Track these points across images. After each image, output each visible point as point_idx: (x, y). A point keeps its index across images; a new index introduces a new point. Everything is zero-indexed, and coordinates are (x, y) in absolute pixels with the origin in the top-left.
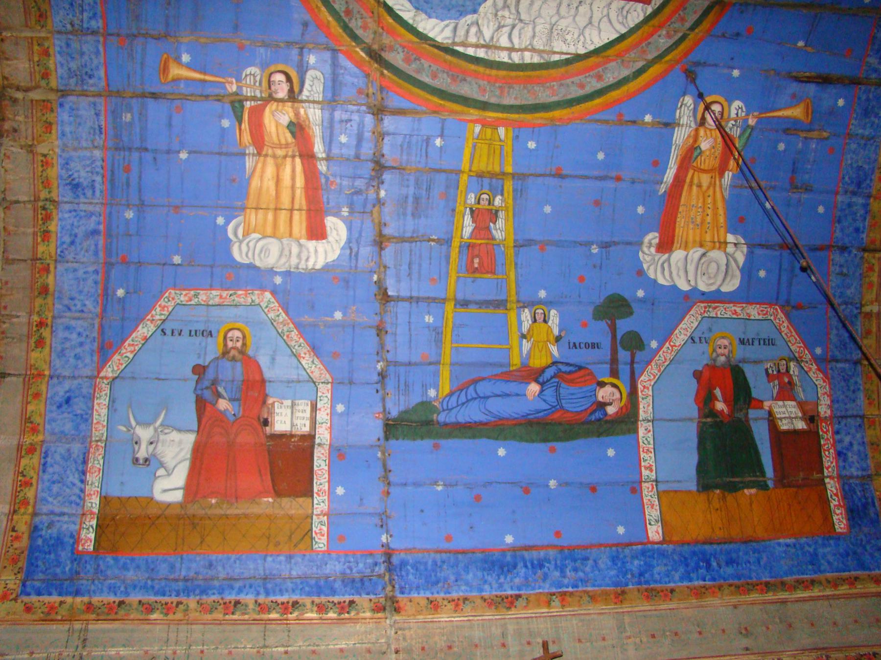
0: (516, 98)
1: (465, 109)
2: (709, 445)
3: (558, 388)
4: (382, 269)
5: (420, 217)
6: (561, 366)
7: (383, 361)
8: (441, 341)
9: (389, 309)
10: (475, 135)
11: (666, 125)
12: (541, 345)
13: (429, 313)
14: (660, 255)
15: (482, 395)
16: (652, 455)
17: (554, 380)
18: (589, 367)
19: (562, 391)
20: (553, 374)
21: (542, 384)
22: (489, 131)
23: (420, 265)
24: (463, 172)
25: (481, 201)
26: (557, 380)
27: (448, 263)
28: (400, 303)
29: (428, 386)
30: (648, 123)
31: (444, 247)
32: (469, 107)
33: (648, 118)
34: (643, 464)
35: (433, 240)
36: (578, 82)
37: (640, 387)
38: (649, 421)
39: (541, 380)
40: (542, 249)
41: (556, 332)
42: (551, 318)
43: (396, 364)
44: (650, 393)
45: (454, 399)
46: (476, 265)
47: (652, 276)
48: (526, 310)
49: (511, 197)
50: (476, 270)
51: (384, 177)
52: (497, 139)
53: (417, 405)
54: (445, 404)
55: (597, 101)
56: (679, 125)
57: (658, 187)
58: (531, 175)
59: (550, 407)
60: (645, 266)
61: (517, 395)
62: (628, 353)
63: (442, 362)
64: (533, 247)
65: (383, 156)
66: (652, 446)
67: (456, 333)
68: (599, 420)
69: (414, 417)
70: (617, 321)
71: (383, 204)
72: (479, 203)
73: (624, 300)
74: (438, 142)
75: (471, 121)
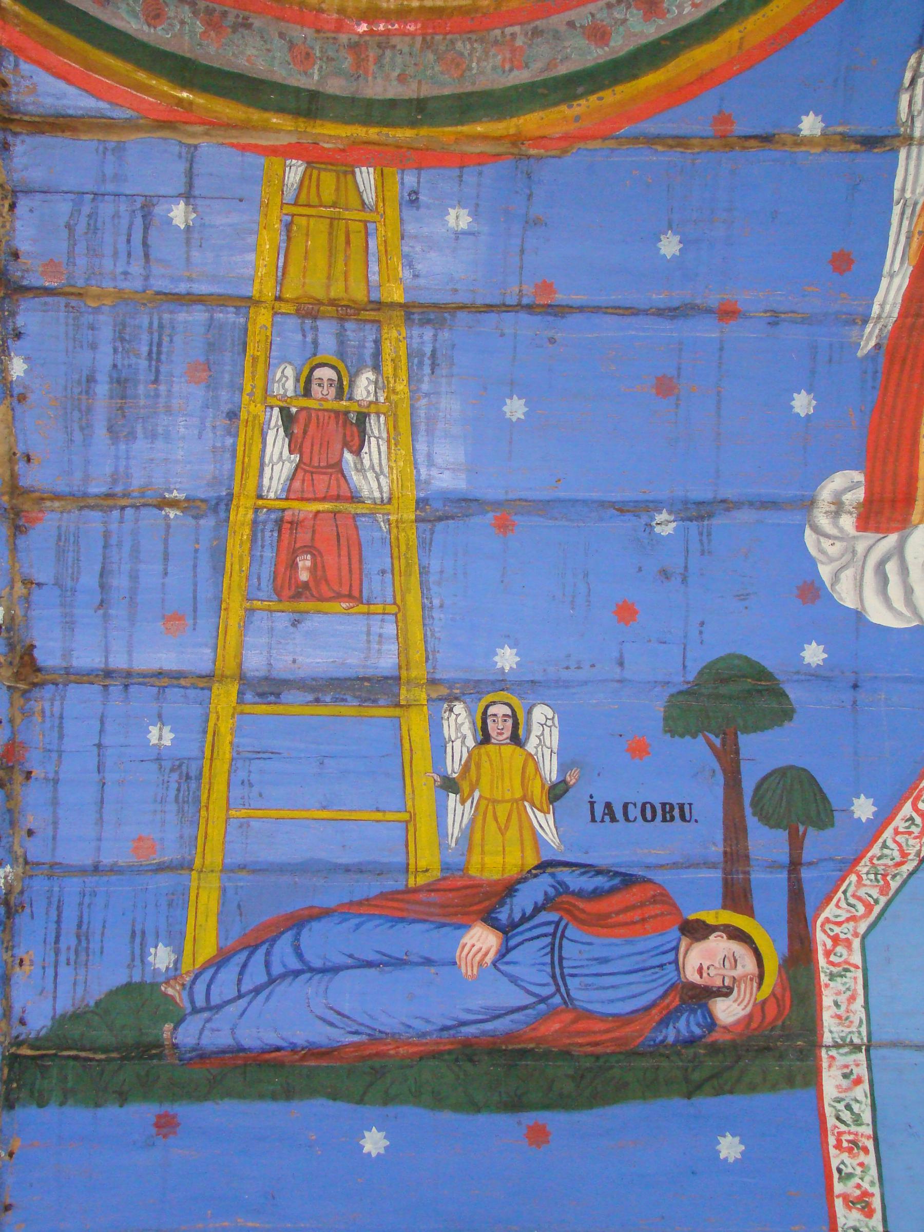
0: (402, 79)
1: (256, 116)
2: (818, 1007)
3: (557, 937)
4: (19, 589)
5: (132, 436)
6: (564, 874)
7: (14, 862)
8: (198, 800)
9: (37, 707)
10: (289, 196)
11: (870, 142)
12: (502, 811)
13: (160, 718)
14: (871, 537)
15: (317, 963)
16: (870, 1160)
17: (544, 916)
18: (658, 877)
19: (569, 950)
20: (540, 899)
21: (506, 930)
22: (328, 179)
23: (134, 576)
24: (258, 303)
25: (315, 387)
26: (554, 916)
27: (219, 568)
28: (74, 692)
29: (150, 938)
30: (810, 141)
31: (208, 522)
32: (265, 109)
33: (810, 125)
34: (838, 1188)
35: (173, 504)
36: (587, 21)
37: (821, 939)
38: (856, 1048)
39: (503, 916)
40: (503, 526)
41: (550, 770)
42: (536, 730)
43: (55, 869)
44: (857, 959)
45: (229, 974)
46: (304, 576)
47: (848, 600)
48: (459, 708)
49: (403, 374)
50: (301, 592)
51: (20, 321)
52: (354, 202)
53: (112, 994)
54: (200, 988)
55: (650, 80)
56: (909, 140)
57: (854, 331)
58: (463, 307)
59: (532, 1000)
60: (825, 572)
61: (428, 962)
62: (782, 835)
63: (197, 863)
64: (477, 520)
65: (16, 255)
66: (869, 1131)
67: (242, 775)
68: (691, 1041)
69: (104, 1036)
70: (743, 739)
71: (22, 398)
72: (307, 393)
73: (761, 673)
74: (179, 214)
75: (273, 151)
